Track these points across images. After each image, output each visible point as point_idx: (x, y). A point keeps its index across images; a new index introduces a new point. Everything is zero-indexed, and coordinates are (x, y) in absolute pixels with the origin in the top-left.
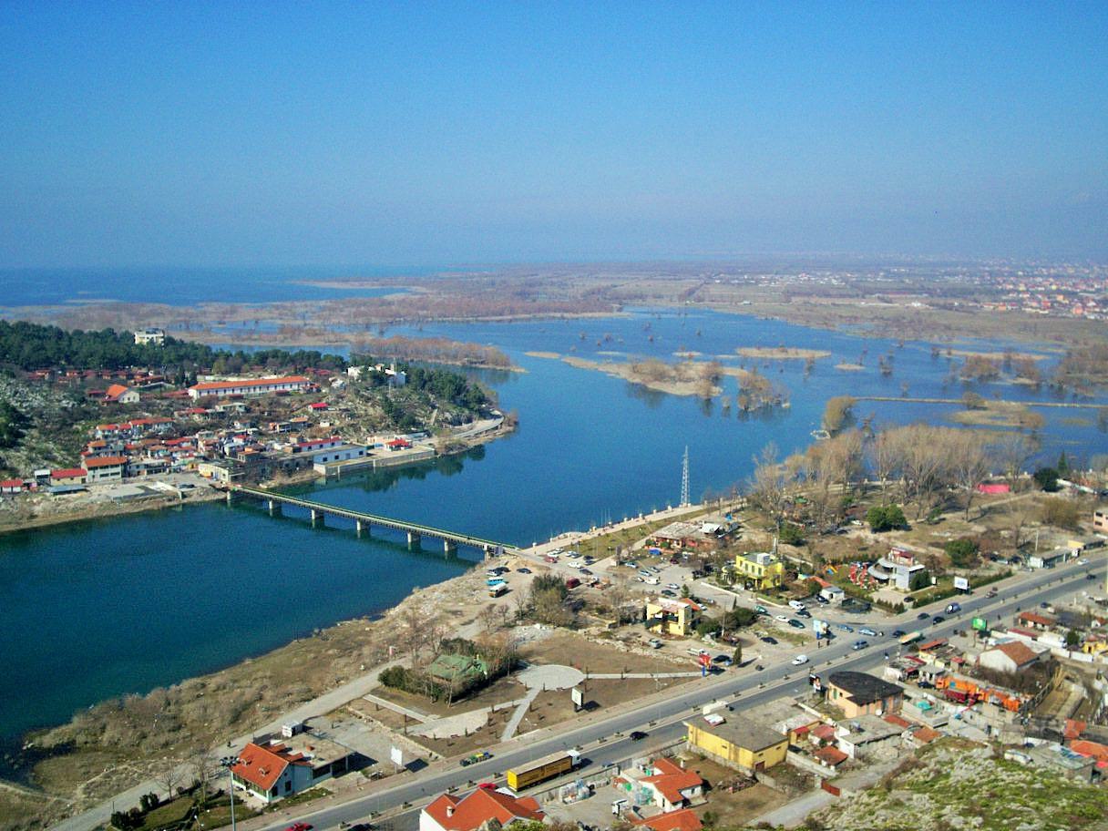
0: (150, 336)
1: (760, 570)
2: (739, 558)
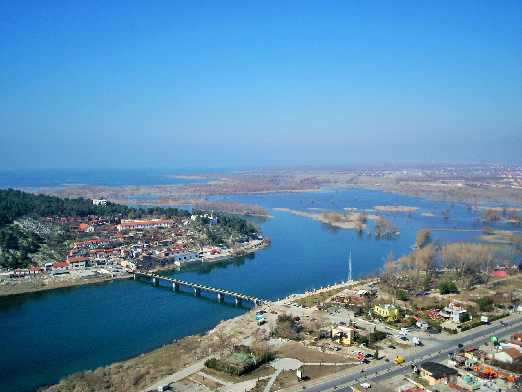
0: (100, 201)
1: (387, 312)
2: (376, 307)
